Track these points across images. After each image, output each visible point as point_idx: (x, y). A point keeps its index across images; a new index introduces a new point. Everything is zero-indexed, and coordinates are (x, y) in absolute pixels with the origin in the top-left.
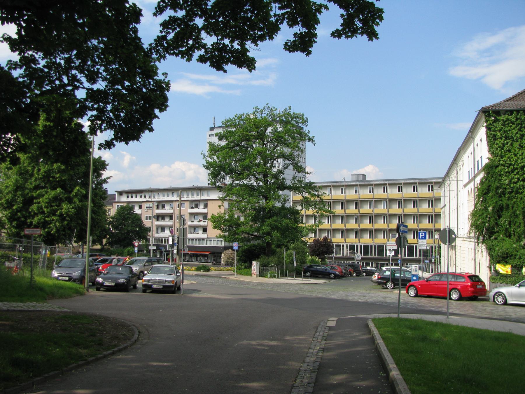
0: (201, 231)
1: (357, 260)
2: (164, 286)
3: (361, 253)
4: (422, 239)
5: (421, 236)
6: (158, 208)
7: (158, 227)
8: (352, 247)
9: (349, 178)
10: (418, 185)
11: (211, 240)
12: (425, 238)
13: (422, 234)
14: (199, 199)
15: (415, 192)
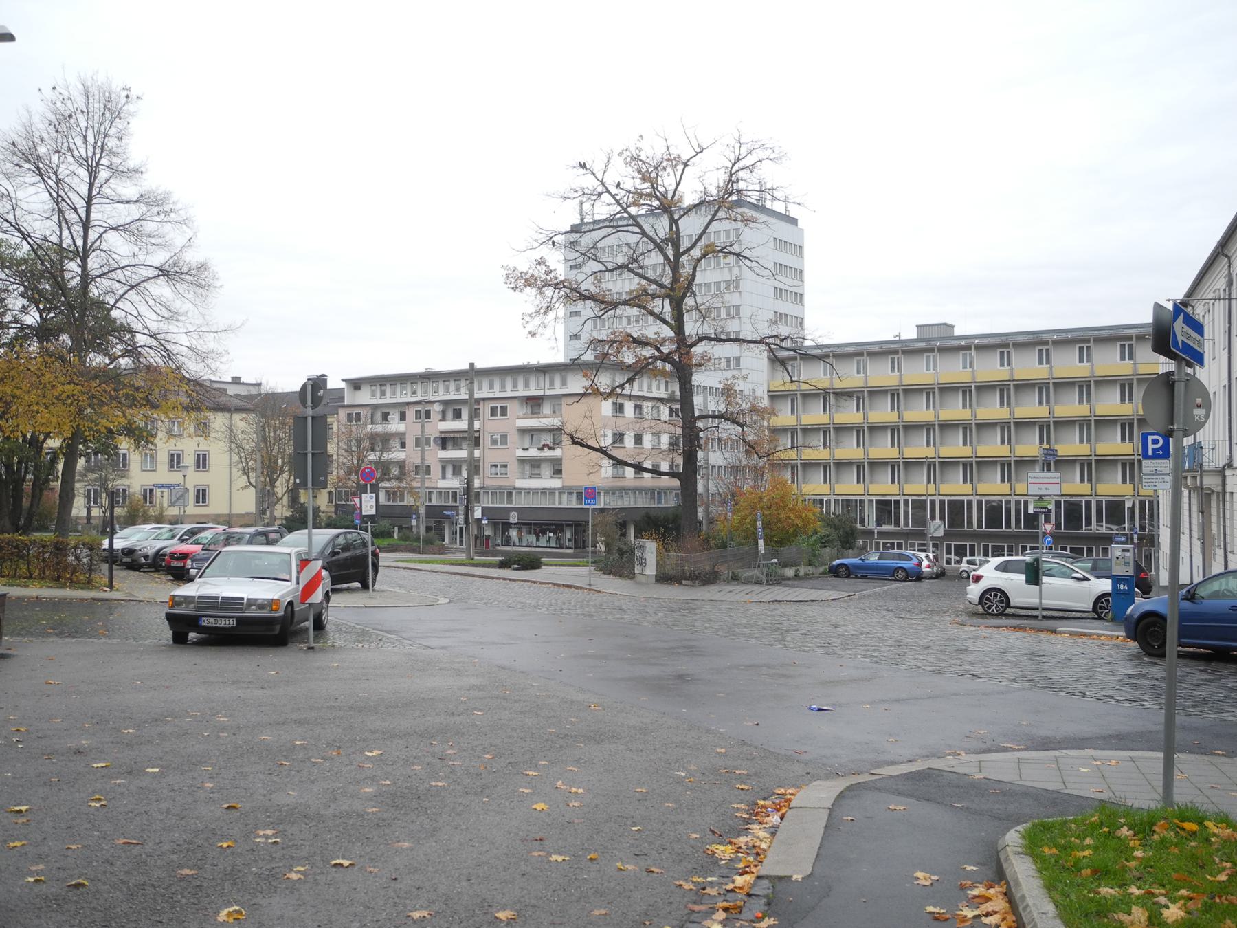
0: (546, 470)
1: (933, 538)
2: (240, 621)
3: (942, 518)
4: (1155, 455)
5: (1151, 446)
6: (443, 419)
7: (444, 464)
8: (919, 505)
9: (910, 334)
10: (1091, 344)
11: (571, 494)
12: (1166, 455)
13: (1155, 442)
14: (540, 393)
15: (1085, 364)
